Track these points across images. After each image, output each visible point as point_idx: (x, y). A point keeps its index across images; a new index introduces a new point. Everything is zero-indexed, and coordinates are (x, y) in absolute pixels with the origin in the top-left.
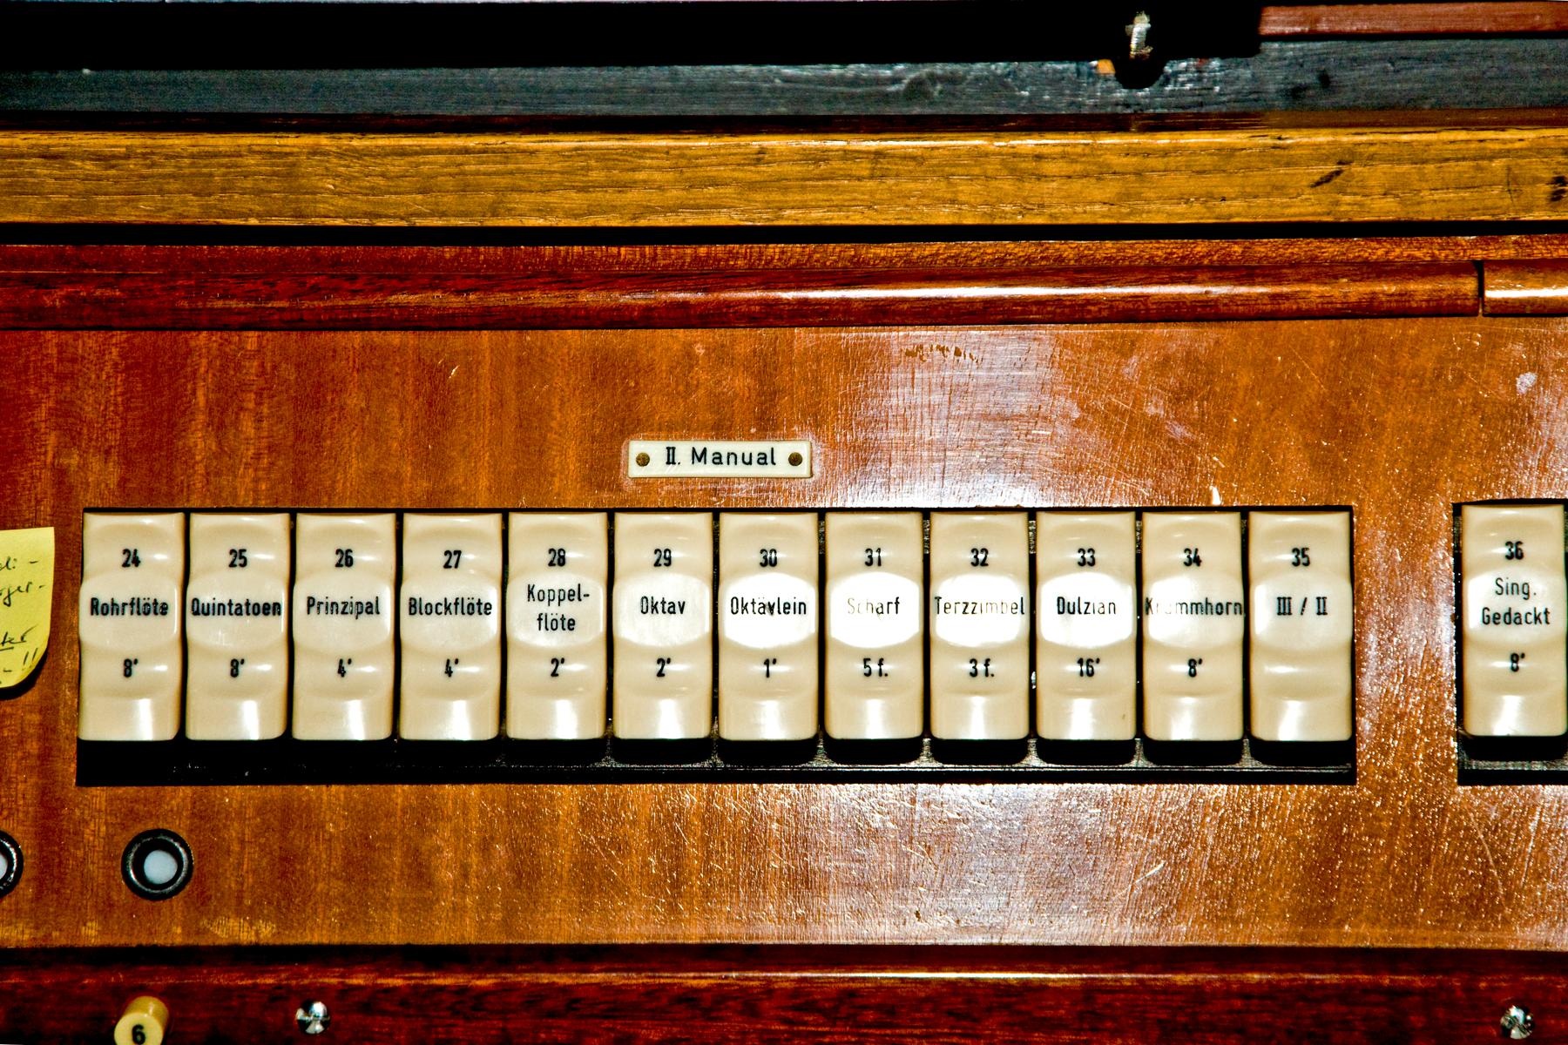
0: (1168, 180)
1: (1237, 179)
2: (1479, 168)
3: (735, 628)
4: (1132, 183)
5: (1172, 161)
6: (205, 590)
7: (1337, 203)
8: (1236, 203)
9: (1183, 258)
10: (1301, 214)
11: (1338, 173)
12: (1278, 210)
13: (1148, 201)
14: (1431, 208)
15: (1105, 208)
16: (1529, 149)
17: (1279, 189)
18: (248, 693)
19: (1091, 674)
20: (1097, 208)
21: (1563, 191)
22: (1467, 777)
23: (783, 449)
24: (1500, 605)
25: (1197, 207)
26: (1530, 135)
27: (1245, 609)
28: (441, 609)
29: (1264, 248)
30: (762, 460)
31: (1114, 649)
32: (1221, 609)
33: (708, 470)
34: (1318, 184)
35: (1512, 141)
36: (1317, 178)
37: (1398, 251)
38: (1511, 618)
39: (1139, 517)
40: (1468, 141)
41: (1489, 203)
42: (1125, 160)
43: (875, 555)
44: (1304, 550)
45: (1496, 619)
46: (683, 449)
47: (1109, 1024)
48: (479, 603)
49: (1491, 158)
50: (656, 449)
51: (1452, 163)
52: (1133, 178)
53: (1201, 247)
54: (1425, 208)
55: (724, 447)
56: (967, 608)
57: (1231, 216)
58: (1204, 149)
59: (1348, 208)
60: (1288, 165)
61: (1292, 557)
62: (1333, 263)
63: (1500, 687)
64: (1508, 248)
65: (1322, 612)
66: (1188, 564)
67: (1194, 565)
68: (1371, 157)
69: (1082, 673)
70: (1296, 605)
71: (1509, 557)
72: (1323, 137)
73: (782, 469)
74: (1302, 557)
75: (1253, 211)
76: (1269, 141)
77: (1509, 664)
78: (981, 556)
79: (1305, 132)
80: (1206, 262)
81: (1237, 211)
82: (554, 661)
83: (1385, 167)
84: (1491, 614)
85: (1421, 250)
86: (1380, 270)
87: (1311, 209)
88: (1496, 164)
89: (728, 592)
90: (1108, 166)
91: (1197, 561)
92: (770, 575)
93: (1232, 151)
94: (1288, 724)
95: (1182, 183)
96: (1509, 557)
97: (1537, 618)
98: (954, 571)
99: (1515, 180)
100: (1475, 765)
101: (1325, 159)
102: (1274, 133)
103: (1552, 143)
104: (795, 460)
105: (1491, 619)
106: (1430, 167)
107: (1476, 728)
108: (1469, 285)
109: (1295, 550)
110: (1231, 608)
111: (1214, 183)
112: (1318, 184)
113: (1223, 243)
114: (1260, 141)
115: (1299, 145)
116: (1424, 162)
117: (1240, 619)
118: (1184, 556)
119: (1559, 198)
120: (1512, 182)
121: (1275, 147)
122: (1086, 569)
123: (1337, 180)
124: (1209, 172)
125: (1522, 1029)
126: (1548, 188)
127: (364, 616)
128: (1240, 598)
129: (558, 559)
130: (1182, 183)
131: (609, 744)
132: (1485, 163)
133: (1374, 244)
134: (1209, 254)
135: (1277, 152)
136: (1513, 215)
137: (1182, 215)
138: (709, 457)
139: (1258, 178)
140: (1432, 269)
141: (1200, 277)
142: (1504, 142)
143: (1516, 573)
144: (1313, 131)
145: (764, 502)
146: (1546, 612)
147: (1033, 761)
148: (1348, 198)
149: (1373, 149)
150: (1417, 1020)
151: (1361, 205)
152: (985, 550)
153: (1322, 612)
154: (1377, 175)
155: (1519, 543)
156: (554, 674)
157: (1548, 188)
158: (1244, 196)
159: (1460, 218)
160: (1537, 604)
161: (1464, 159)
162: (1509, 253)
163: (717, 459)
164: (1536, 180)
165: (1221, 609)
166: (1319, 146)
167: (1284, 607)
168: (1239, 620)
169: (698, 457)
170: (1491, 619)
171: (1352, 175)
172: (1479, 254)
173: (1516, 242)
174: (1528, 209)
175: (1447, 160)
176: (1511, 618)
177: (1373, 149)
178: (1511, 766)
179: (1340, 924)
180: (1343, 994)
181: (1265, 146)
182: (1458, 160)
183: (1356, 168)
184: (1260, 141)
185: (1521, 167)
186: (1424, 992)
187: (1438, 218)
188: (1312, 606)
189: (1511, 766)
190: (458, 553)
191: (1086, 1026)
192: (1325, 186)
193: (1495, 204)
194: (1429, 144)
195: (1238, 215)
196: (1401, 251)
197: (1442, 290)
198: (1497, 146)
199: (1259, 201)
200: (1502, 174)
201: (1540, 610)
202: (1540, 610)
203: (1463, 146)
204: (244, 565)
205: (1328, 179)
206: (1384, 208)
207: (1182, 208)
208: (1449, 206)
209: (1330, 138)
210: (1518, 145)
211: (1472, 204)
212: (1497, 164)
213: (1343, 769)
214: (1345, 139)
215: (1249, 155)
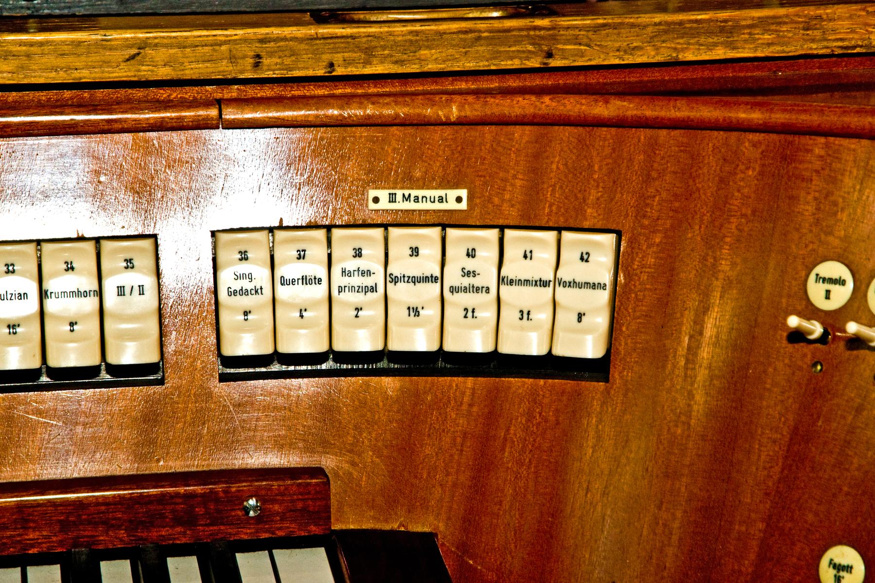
0: (44, 60)
1: (83, 58)
2: (214, 50)
3: (283, 292)
4: (24, 60)
5: (46, 49)
6: (395, 269)
7: (139, 71)
8: (84, 71)
9: (57, 101)
10: (116, 77)
11: (138, 54)
12: (107, 75)
13: (34, 71)
14: (191, 71)
15: (10, 75)
16: (240, 40)
17: (107, 63)
18: (363, 326)
19: (15, 333)
20: (5, 75)
21: (259, 62)
22: (224, 378)
23: (453, 194)
24: (237, 285)
25: (62, 73)
26: (240, 32)
27: (100, 293)
28: (253, 292)
29: (100, 93)
30: (441, 200)
31: (27, 318)
32: (86, 294)
33: (411, 206)
34: (128, 60)
35: (231, 36)
36: (127, 57)
37: (174, 95)
38: (243, 292)
39: (386, 229)
40: (207, 36)
41: (221, 69)
42: (19, 48)
43: (302, 253)
44: (131, 260)
45: (235, 292)
46: (399, 193)
47: (31, 525)
48: (315, 278)
49: (220, 45)
50: (383, 194)
51: (200, 48)
52: (25, 58)
53: (67, 94)
54: (187, 72)
55: (420, 193)
56: (78, 294)
57: (81, 78)
58: (63, 42)
59: (145, 72)
60: (110, 49)
61: (125, 264)
62: (140, 101)
63: (240, 329)
64: (233, 91)
65: (142, 293)
66: (67, 270)
67: (70, 271)
68: (156, 45)
69: (10, 333)
70: (127, 291)
71: (241, 260)
72: (129, 35)
73: (452, 205)
74: (129, 264)
75: (93, 75)
76: (99, 37)
77: (242, 317)
78: (11, 268)
79: (119, 31)
80: (70, 103)
81: (86, 76)
82: (357, 309)
83: (164, 50)
84: (232, 290)
85: (190, 93)
86: (167, 105)
87: (125, 74)
88: (224, 48)
89: (278, 274)
90: (11, 52)
91: (72, 268)
92: (70, 276)
93: (79, 43)
94: (128, 354)
95: (52, 60)
96: (241, 260)
97: (256, 292)
98: (55, 274)
99: (234, 57)
100: (229, 371)
101: (131, 47)
102: (102, 32)
103: (252, 36)
104: (376, 200)
105: (232, 293)
106: (188, 50)
107: (229, 350)
108: (213, 112)
109: (126, 260)
110: (92, 293)
111: (69, 60)
112: (128, 60)
113: (79, 92)
114: (94, 37)
115: (116, 39)
116: (185, 47)
117: (97, 299)
118: (65, 266)
119: (257, 66)
120: (232, 59)
121: (103, 40)
122: (11, 277)
123: (138, 58)
124: (67, 55)
125: (255, 511)
126: (252, 61)
127: (369, 294)
128: (96, 288)
129: (358, 253)
130: (52, 60)
131: (277, 356)
132: (217, 48)
133: (162, 91)
134: (72, 98)
135: (104, 43)
136: (234, 75)
137: (54, 78)
138: (412, 198)
139: (95, 58)
140: (194, 104)
141: (67, 111)
142: (227, 36)
143: (244, 268)
144: (124, 31)
145: (408, 221)
146: (261, 288)
147: (44, 379)
148: (144, 68)
149: (156, 41)
150: (200, 510)
151: (152, 71)
152: (13, 265)
153: (142, 293)
154: (161, 55)
155: (246, 252)
156: (357, 316)
157: (252, 61)
158: (87, 67)
159: (206, 78)
160: (257, 283)
161: (206, 45)
162: (234, 95)
163: (417, 199)
164: (244, 57)
165: (86, 294)
166: (127, 39)
167: (121, 291)
168: (96, 300)
169: (406, 198)
170: (232, 293)
171: (146, 55)
172: (219, 96)
173: (238, 89)
174: (242, 72)
175: (197, 46)
176: (243, 292)
177: (156, 41)
178: (242, 370)
179: (158, 461)
180: (206, 498)
181: (97, 39)
182: (203, 46)
183: (148, 51)
184: (94, 37)
185: (237, 50)
186: (203, 495)
187: (194, 77)
188: (136, 291)
189: (242, 370)
190: (304, 251)
191: (19, 526)
192: (132, 62)
193: (224, 69)
194: (187, 37)
195: (85, 78)
196: (175, 94)
197: (199, 116)
198: (223, 38)
199: (96, 70)
200: (227, 54)
201: (258, 287)
202: (258, 287)
203: (205, 38)
204: (417, 256)
205: (133, 57)
206: (164, 73)
207: (53, 74)
208: (201, 71)
209: (133, 35)
210: (236, 37)
211: (211, 70)
212: (224, 48)
213: (159, 376)
214: (141, 35)
215: (89, 45)
